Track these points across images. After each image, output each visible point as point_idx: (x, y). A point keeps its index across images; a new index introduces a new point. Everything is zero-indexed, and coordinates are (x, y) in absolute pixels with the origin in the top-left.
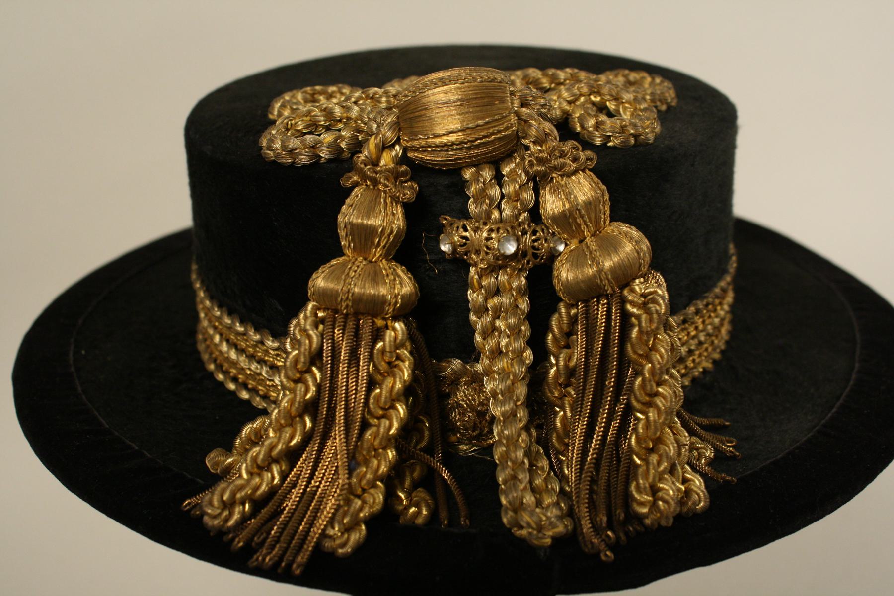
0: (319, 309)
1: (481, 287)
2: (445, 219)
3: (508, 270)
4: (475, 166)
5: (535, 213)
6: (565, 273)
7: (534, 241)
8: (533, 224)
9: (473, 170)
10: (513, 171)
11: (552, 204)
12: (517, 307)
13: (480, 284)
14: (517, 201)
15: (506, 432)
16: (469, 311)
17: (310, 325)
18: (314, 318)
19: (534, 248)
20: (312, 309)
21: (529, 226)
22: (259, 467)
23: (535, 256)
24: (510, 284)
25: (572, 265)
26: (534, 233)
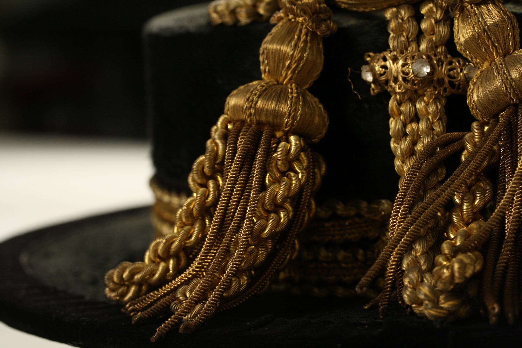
0: (230, 122)
1: (400, 113)
2: (369, 56)
3: (425, 98)
4: (395, 6)
5: (450, 43)
6: (475, 95)
7: (450, 70)
8: (449, 56)
9: (394, 9)
10: (430, 10)
11: (463, 33)
12: (433, 129)
13: (399, 110)
14: (433, 34)
15: (259, 103)
16: (390, 137)
17: (219, 135)
18: (224, 130)
19: (449, 76)
20: (223, 120)
21: (446, 57)
22: (159, 257)
23: (451, 84)
24: (427, 110)
25: (490, 100)
26: (450, 63)
